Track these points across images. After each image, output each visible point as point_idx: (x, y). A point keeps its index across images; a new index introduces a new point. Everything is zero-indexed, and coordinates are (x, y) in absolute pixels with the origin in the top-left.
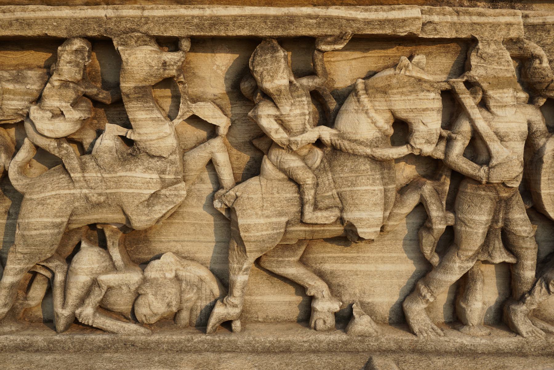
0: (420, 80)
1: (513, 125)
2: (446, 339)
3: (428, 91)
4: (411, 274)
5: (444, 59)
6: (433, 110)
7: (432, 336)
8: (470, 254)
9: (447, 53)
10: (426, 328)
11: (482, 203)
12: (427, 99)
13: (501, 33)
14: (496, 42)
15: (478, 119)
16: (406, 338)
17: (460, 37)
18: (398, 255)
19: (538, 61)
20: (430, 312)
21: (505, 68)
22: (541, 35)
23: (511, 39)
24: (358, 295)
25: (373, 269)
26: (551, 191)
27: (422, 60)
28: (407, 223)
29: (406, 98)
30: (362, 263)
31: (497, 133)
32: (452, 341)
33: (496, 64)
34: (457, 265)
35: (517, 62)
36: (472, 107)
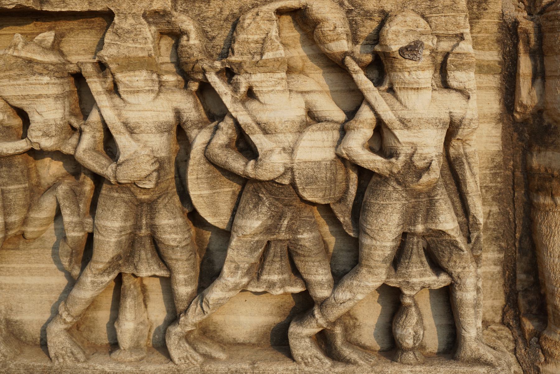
0: (30, 61)
1: (148, 114)
2: (85, 365)
3: (41, 74)
4: (63, 288)
5: (88, 36)
6: (48, 96)
7: (69, 362)
8: (101, 266)
9: (91, 29)
10: (64, 352)
11: (115, 207)
12: (39, 84)
13: (141, 5)
14: (134, 16)
15: (103, 107)
16: (39, 364)
17: (95, 9)
18: (47, 265)
19: (185, 38)
20: (92, 332)
21: (142, 46)
22: (200, 7)
23: (156, 12)
24: (3, 312)
25: (20, 282)
26: (202, 193)
27: (47, 38)
28: (55, 229)
29: (15, 83)
30: (6, 275)
31: (126, 125)
32: (91, 368)
33: (131, 42)
34: (89, 279)
35: (173, 39)
36: (99, 93)
